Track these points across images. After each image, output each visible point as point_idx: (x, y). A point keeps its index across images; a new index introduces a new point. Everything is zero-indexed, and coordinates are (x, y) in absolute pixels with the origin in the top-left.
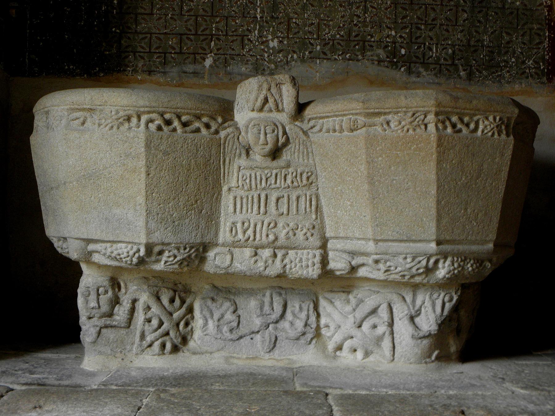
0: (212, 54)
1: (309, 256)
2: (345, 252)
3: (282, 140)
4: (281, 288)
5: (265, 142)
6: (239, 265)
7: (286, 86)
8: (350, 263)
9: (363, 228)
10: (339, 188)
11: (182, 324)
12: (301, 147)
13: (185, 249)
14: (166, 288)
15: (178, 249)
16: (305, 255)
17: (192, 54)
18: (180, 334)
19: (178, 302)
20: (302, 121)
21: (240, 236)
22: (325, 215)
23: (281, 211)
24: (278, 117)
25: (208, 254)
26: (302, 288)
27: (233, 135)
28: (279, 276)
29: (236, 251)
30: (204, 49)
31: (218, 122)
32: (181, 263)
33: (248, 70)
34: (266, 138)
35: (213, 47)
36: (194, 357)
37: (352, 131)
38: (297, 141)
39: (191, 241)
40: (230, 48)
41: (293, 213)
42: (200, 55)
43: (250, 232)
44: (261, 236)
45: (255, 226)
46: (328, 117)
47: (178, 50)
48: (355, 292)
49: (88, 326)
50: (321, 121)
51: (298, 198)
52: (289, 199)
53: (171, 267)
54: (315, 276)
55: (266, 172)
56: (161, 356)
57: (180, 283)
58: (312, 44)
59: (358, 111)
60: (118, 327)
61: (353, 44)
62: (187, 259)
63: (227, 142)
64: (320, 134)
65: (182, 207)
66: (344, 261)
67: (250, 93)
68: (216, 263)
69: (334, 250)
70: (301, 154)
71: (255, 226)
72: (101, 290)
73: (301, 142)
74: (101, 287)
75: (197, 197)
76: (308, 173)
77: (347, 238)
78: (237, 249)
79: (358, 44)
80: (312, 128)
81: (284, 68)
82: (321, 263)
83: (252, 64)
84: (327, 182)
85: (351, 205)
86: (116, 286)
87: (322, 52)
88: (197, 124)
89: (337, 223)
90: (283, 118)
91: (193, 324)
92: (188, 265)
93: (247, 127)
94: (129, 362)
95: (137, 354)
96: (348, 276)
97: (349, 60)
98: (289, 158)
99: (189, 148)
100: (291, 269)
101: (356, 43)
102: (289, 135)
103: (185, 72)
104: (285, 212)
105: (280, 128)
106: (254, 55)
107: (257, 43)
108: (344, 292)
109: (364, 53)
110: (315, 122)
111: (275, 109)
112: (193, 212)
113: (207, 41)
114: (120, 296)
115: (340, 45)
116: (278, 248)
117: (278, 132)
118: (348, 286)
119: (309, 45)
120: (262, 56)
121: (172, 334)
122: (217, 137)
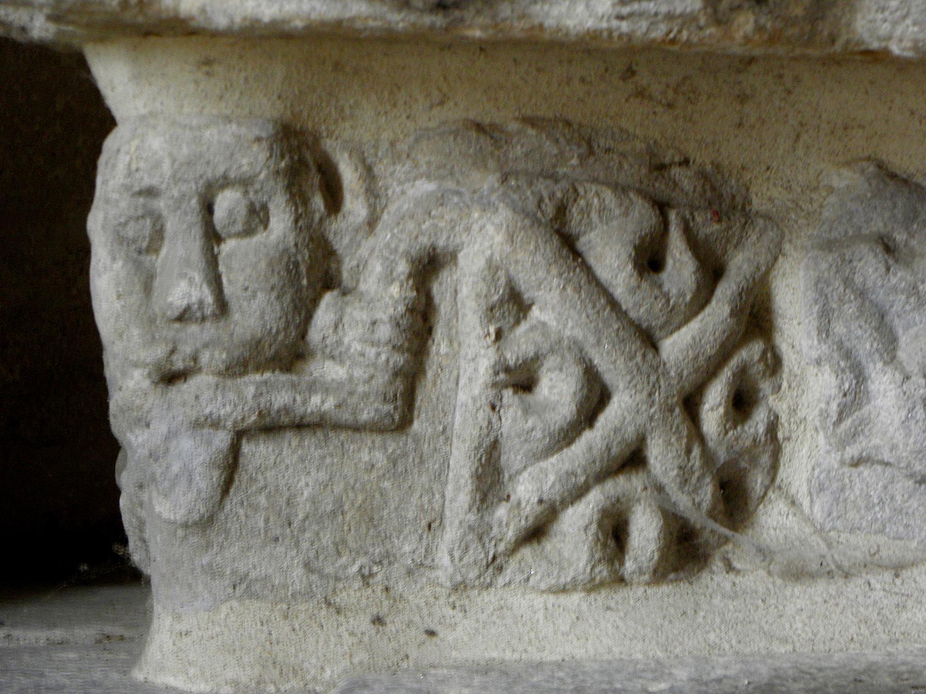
11: (715, 398)
14: (607, 184)
18: (708, 457)
19: (681, 269)
36: (800, 597)
49: (160, 428)
56: (601, 597)
57: (685, 162)
60: (338, 427)
72: (227, 203)
74: (225, 182)
86: (315, 179)
91: (774, 402)
94: (416, 634)
95: (460, 587)
114: (340, 244)
121: (661, 456)
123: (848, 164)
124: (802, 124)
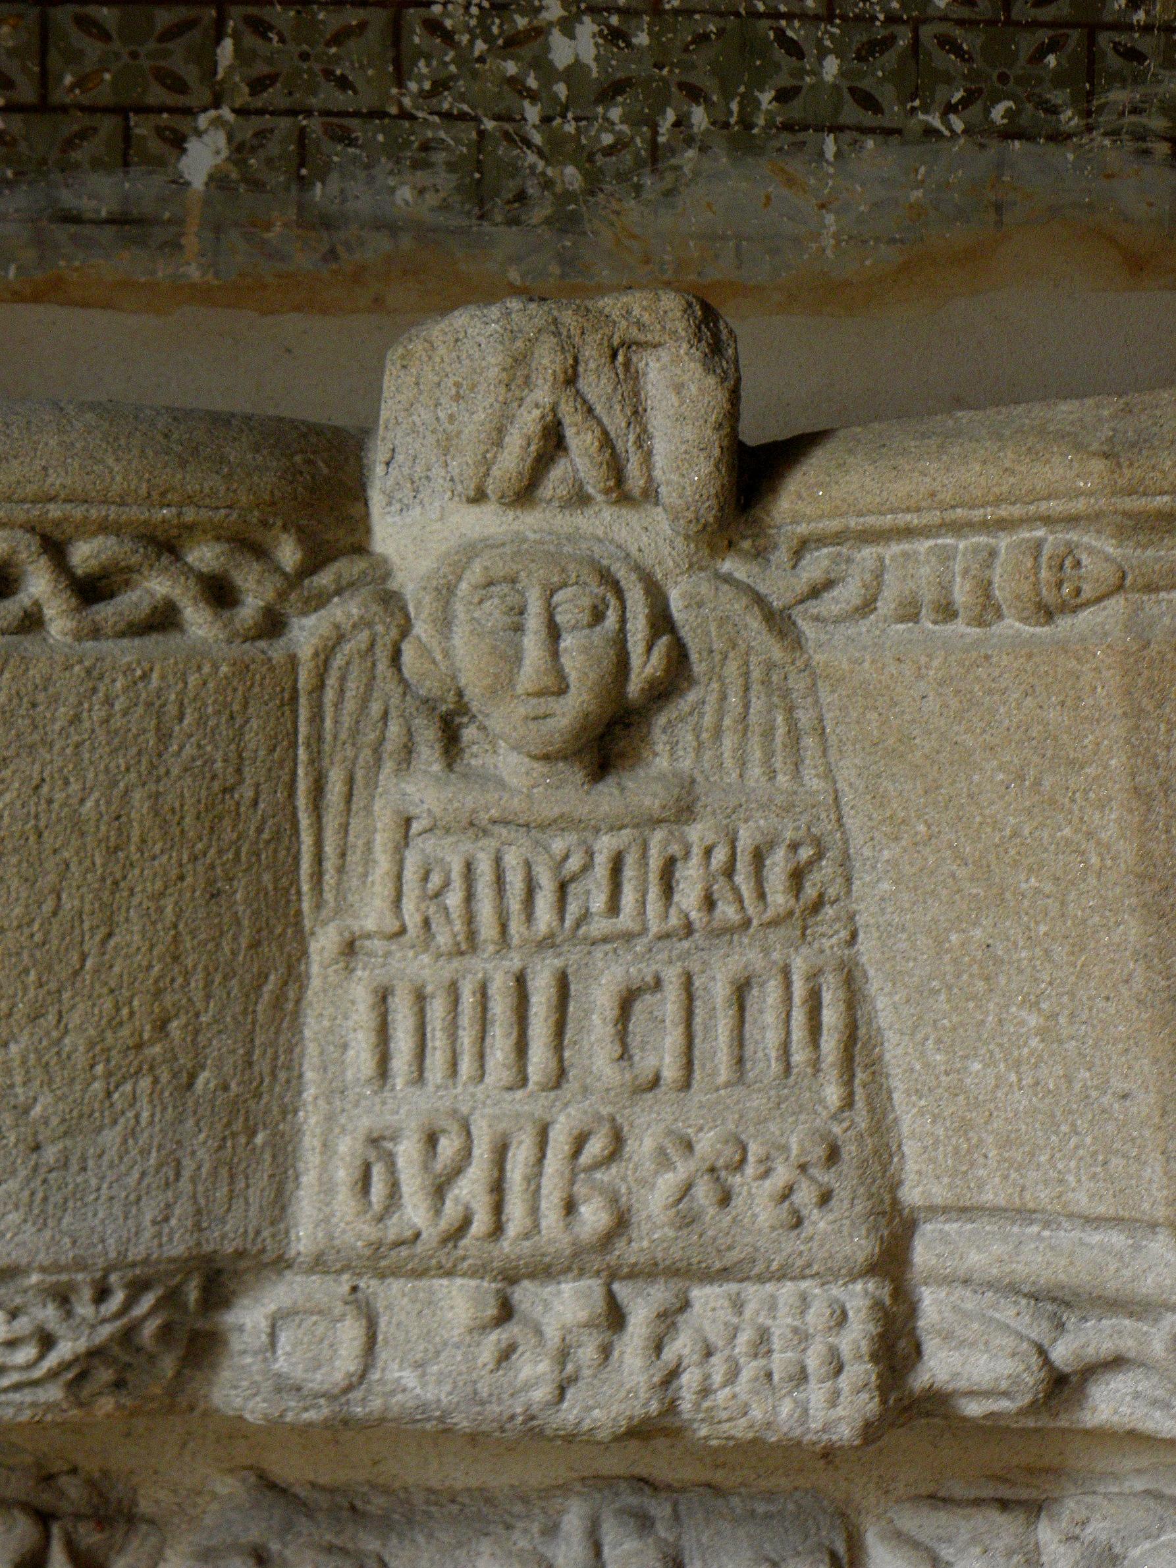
0: (226, 113)
1: (810, 1317)
2: (1011, 1289)
3: (646, 665)
4: (644, 1483)
5: (549, 681)
6: (409, 1378)
7: (663, 353)
8: (1042, 1351)
9: (1116, 1162)
10: (977, 933)
12: (757, 705)
13: (102, 1294)
15: (63, 1298)
16: (782, 1310)
17: (106, 110)
20: (760, 555)
21: (415, 1211)
22: (894, 1083)
23: (646, 1063)
24: (622, 534)
25: (230, 1318)
26: (764, 1484)
27: (364, 636)
28: (640, 1432)
29: (394, 1297)
30: (178, 85)
31: (278, 569)
32: (82, 1376)
33: (431, 199)
34: (555, 654)
35: (231, 68)
37: (1047, 613)
38: (732, 668)
39: (136, 1253)
40: (328, 74)
41: (714, 1073)
42: (154, 120)
43: (470, 1189)
44: (534, 1210)
45: (501, 1152)
46: (908, 533)
47: (26, 92)
48: (1071, 1507)
50: (867, 553)
51: (741, 991)
52: (690, 997)
53: (26, 1396)
54: (845, 1433)
55: (558, 845)
57: (74, 1471)
58: (794, 49)
59: (1080, 505)
61: (1026, 44)
62: (116, 1350)
63: (332, 681)
64: (864, 625)
65: (81, 1059)
66: (1009, 1342)
67: (458, 397)
68: (281, 1364)
69: (948, 1281)
70: (755, 741)
71: (501, 1152)
73: (756, 674)
75: (168, 999)
76: (794, 847)
77: (1024, 1214)
78: (396, 1286)
79: (1053, 46)
80: (815, 592)
81: (638, 188)
82: (875, 1357)
83: (451, 167)
84: (906, 897)
85: (1043, 1033)
87: (852, 90)
88: (158, 586)
89: (965, 1126)
90: (651, 536)
92: (119, 1385)
93: (446, 593)
96: (1031, 1423)
97: (1007, 134)
98: (686, 764)
99: (118, 722)
100: (705, 1391)
101: (1044, 35)
102: (685, 633)
103: (71, 218)
104: (671, 1072)
105: (636, 597)
106: (463, 116)
107: (480, 46)
108: (1004, 1505)
109: (1090, 94)
110: (835, 560)
111: (607, 491)
112: (145, 1083)
113: (194, 36)
115: (957, 50)
116: (633, 1275)
117: (623, 620)
118: (1030, 1470)
119: (779, 54)
120: (510, 119)
122: (277, 651)
123: (231, 1471)
124: (189, 1433)
